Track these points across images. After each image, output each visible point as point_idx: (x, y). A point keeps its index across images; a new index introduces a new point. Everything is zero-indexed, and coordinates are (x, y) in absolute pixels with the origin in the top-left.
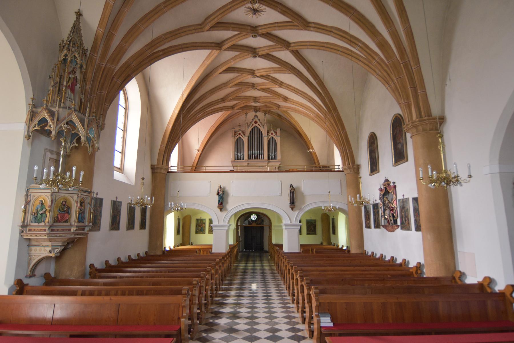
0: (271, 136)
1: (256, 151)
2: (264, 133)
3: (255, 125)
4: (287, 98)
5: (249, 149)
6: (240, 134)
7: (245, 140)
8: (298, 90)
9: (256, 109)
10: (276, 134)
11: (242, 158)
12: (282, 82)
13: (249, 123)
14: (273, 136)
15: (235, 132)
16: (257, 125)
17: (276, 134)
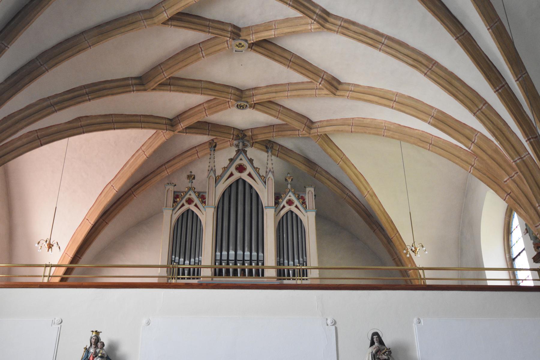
0: (288, 208)
1: (240, 252)
2: (266, 196)
3: (237, 175)
4: (339, 82)
5: (218, 245)
6: (190, 201)
7: (207, 217)
8: (377, 33)
9: (243, 137)
10: (304, 203)
11: (195, 272)
12: (328, 14)
13: (219, 172)
14: (293, 208)
15: (177, 196)
16: (244, 176)
17: (304, 203)
